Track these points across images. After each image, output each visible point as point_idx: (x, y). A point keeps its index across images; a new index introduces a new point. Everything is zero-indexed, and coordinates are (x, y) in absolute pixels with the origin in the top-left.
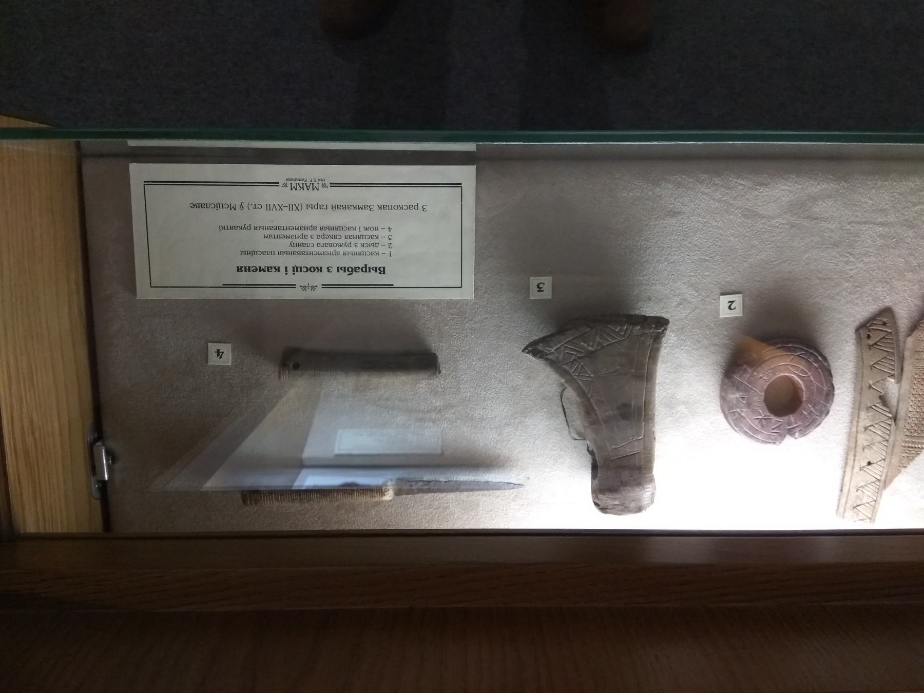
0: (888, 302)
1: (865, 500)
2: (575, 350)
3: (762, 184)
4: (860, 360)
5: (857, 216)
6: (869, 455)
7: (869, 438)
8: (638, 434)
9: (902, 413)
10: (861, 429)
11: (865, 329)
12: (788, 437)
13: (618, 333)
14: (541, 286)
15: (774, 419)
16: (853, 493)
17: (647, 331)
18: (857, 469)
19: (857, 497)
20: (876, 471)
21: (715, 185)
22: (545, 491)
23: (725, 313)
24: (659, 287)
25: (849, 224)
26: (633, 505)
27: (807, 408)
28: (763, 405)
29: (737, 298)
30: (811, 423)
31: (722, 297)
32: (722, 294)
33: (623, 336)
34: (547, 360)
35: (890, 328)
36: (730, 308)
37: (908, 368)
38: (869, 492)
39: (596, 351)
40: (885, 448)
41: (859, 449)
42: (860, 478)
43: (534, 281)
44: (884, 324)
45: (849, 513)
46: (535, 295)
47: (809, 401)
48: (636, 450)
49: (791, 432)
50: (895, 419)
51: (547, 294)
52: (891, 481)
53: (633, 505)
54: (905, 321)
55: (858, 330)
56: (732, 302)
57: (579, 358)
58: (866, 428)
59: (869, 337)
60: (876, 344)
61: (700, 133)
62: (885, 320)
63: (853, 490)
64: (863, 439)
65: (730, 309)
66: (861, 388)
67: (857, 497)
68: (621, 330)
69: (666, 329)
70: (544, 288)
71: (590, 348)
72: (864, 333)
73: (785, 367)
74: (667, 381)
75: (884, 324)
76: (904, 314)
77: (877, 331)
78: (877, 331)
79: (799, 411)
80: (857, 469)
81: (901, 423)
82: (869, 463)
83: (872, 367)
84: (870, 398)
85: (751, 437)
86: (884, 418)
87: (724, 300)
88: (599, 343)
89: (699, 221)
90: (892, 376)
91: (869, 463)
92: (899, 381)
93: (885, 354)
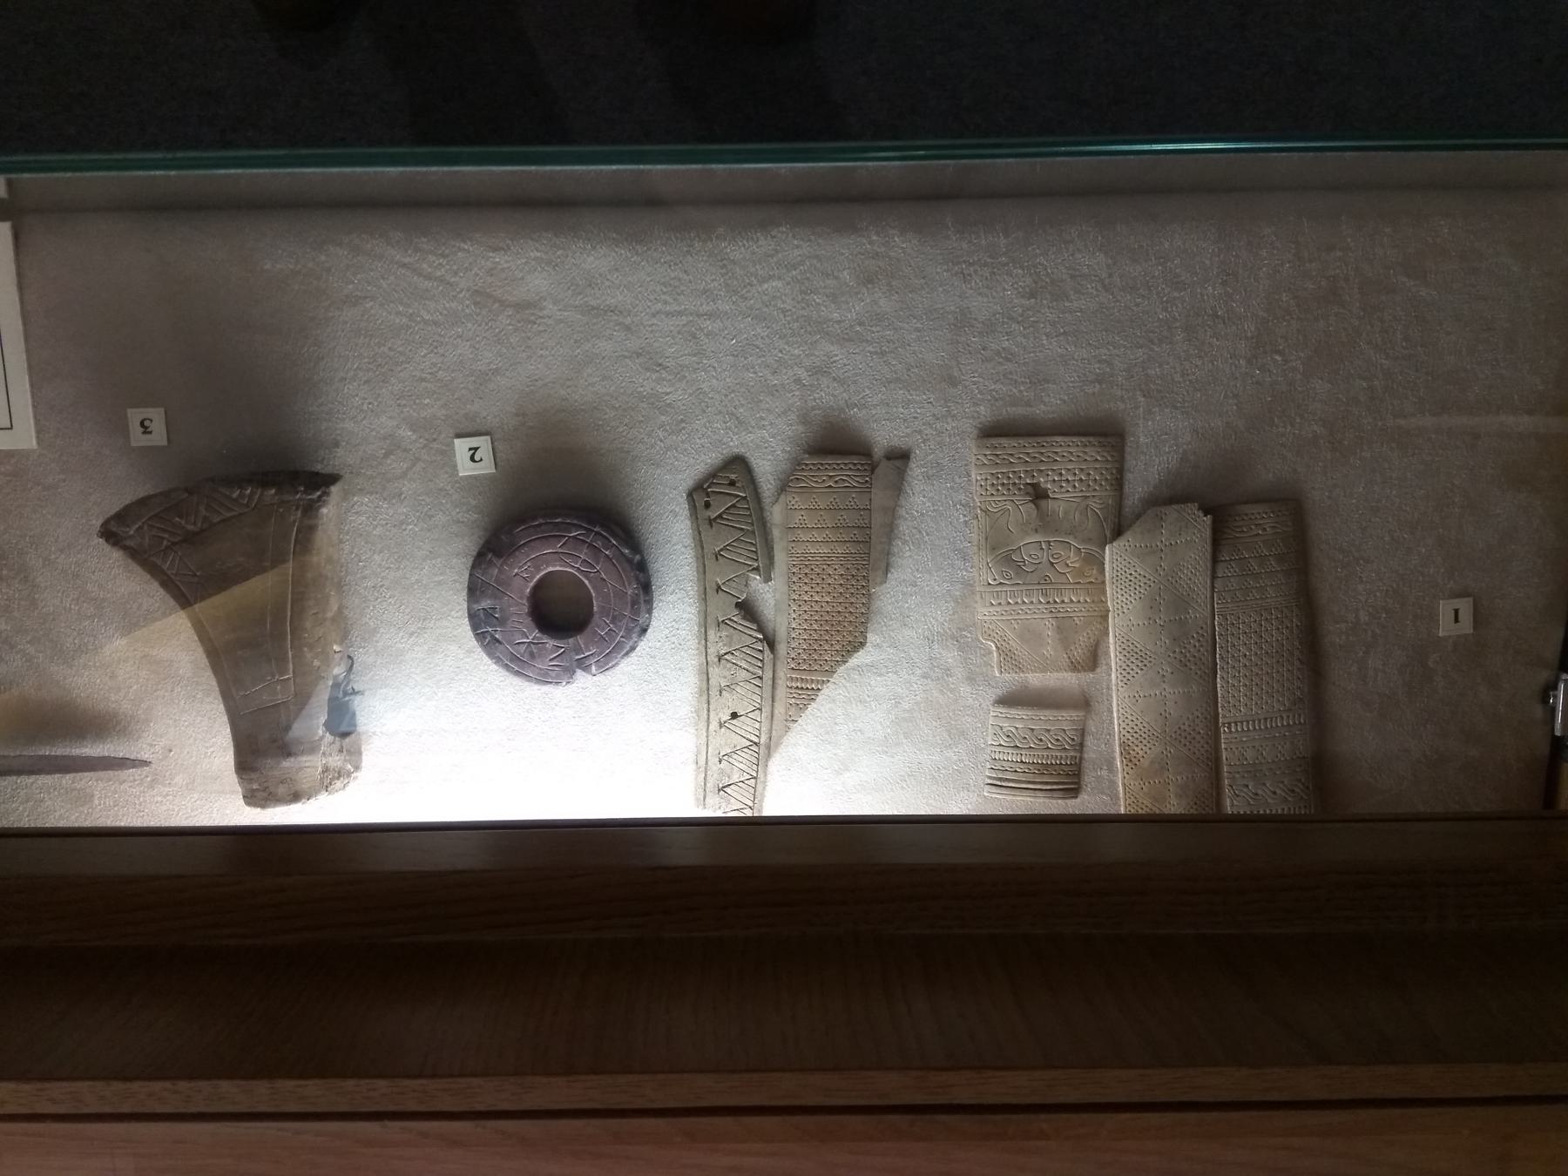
0: (735, 444)
1: (735, 778)
2: (164, 531)
3: (495, 250)
4: (700, 544)
5: (666, 303)
6: (730, 702)
7: (727, 673)
8: (283, 671)
9: (782, 633)
10: (712, 658)
11: (701, 494)
12: (579, 672)
13: (235, 500)
14: (147, 423)
15: (550, 643)
16: (714, 767)
17: (287, 497)
18: (714, 725)
19: (722, 772)
20: (746, 726)
21: (417, 250)
22: (184, 778)
23: (466, 469)
24: (349, 425)
25: (654, 315)
26: (281, 790)
27: (600, 625)
28: (528, 620)
29: (483, 443)
30: (612, 650)
31: (457, 441)
32: (459, 436)
33: (247, 506)
34: (125, 548)
35: (743, 489)
36: (472, 459)
37: (780, 557)
38: (743, 762)
39: (202, 531)
40: (757, 690)
41: (714, 692)
42: (724, 741)
43: (135, 416)
44: (732, 483)
45: (713, 800)
46: (138, 439)
47: (605, 612)
48: (280, 699)
49: (583, 665)
50: (771, 643)
51: (159, 437)
52: (778, 744)
53: (281, 790)
54: (770, 478)
55: (690, 495)
56: (476, 449)
57: (174, 544)
58: (720, 658)
59: (707, 505)
60: (720, 516)
61: (205, 155)
62: (733, 476)
63: (713, 760)
64: (718, 675)
65: (471, 460)
66: (708, 592)
67: (722, 772)
68: (241, 496)
69: (326, 494)
70: (154, 427)
71: (190, 527)
72: (700, 500)
73: (545, 561)
74: (386, 583)
75: (732, 483)
76: (766, 468)
77: (726, 495)
78: (726, 495)
79: (588, 631)
80: (714, 725)
81: (782, 649)
82: (734, 716)
83: (717, 556)
84: (723, 608)
85: (518, 673)
86: (749, 641)
87: (462, 446)
88: (205, 519)
89: (398, 313)
90: (757, 569)
91: (734, 716)
92: (768, 579)
93: (738, 534)
